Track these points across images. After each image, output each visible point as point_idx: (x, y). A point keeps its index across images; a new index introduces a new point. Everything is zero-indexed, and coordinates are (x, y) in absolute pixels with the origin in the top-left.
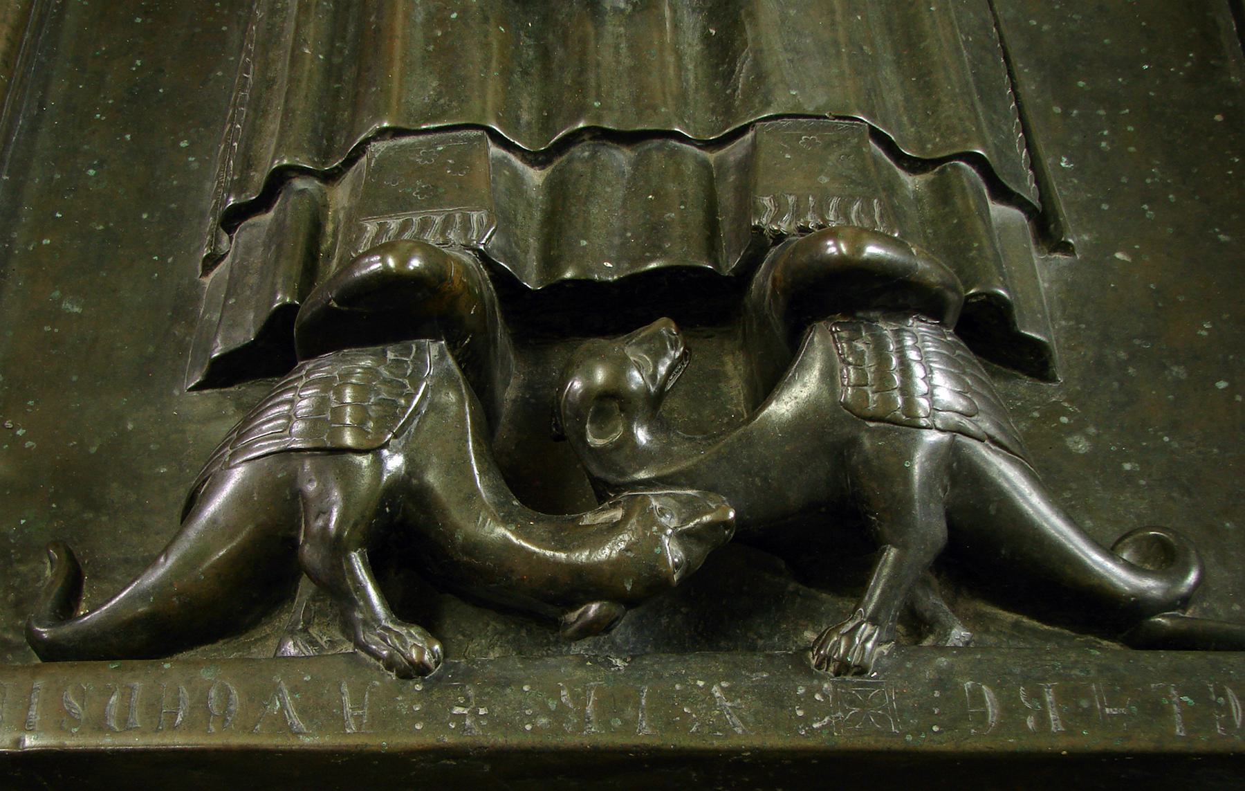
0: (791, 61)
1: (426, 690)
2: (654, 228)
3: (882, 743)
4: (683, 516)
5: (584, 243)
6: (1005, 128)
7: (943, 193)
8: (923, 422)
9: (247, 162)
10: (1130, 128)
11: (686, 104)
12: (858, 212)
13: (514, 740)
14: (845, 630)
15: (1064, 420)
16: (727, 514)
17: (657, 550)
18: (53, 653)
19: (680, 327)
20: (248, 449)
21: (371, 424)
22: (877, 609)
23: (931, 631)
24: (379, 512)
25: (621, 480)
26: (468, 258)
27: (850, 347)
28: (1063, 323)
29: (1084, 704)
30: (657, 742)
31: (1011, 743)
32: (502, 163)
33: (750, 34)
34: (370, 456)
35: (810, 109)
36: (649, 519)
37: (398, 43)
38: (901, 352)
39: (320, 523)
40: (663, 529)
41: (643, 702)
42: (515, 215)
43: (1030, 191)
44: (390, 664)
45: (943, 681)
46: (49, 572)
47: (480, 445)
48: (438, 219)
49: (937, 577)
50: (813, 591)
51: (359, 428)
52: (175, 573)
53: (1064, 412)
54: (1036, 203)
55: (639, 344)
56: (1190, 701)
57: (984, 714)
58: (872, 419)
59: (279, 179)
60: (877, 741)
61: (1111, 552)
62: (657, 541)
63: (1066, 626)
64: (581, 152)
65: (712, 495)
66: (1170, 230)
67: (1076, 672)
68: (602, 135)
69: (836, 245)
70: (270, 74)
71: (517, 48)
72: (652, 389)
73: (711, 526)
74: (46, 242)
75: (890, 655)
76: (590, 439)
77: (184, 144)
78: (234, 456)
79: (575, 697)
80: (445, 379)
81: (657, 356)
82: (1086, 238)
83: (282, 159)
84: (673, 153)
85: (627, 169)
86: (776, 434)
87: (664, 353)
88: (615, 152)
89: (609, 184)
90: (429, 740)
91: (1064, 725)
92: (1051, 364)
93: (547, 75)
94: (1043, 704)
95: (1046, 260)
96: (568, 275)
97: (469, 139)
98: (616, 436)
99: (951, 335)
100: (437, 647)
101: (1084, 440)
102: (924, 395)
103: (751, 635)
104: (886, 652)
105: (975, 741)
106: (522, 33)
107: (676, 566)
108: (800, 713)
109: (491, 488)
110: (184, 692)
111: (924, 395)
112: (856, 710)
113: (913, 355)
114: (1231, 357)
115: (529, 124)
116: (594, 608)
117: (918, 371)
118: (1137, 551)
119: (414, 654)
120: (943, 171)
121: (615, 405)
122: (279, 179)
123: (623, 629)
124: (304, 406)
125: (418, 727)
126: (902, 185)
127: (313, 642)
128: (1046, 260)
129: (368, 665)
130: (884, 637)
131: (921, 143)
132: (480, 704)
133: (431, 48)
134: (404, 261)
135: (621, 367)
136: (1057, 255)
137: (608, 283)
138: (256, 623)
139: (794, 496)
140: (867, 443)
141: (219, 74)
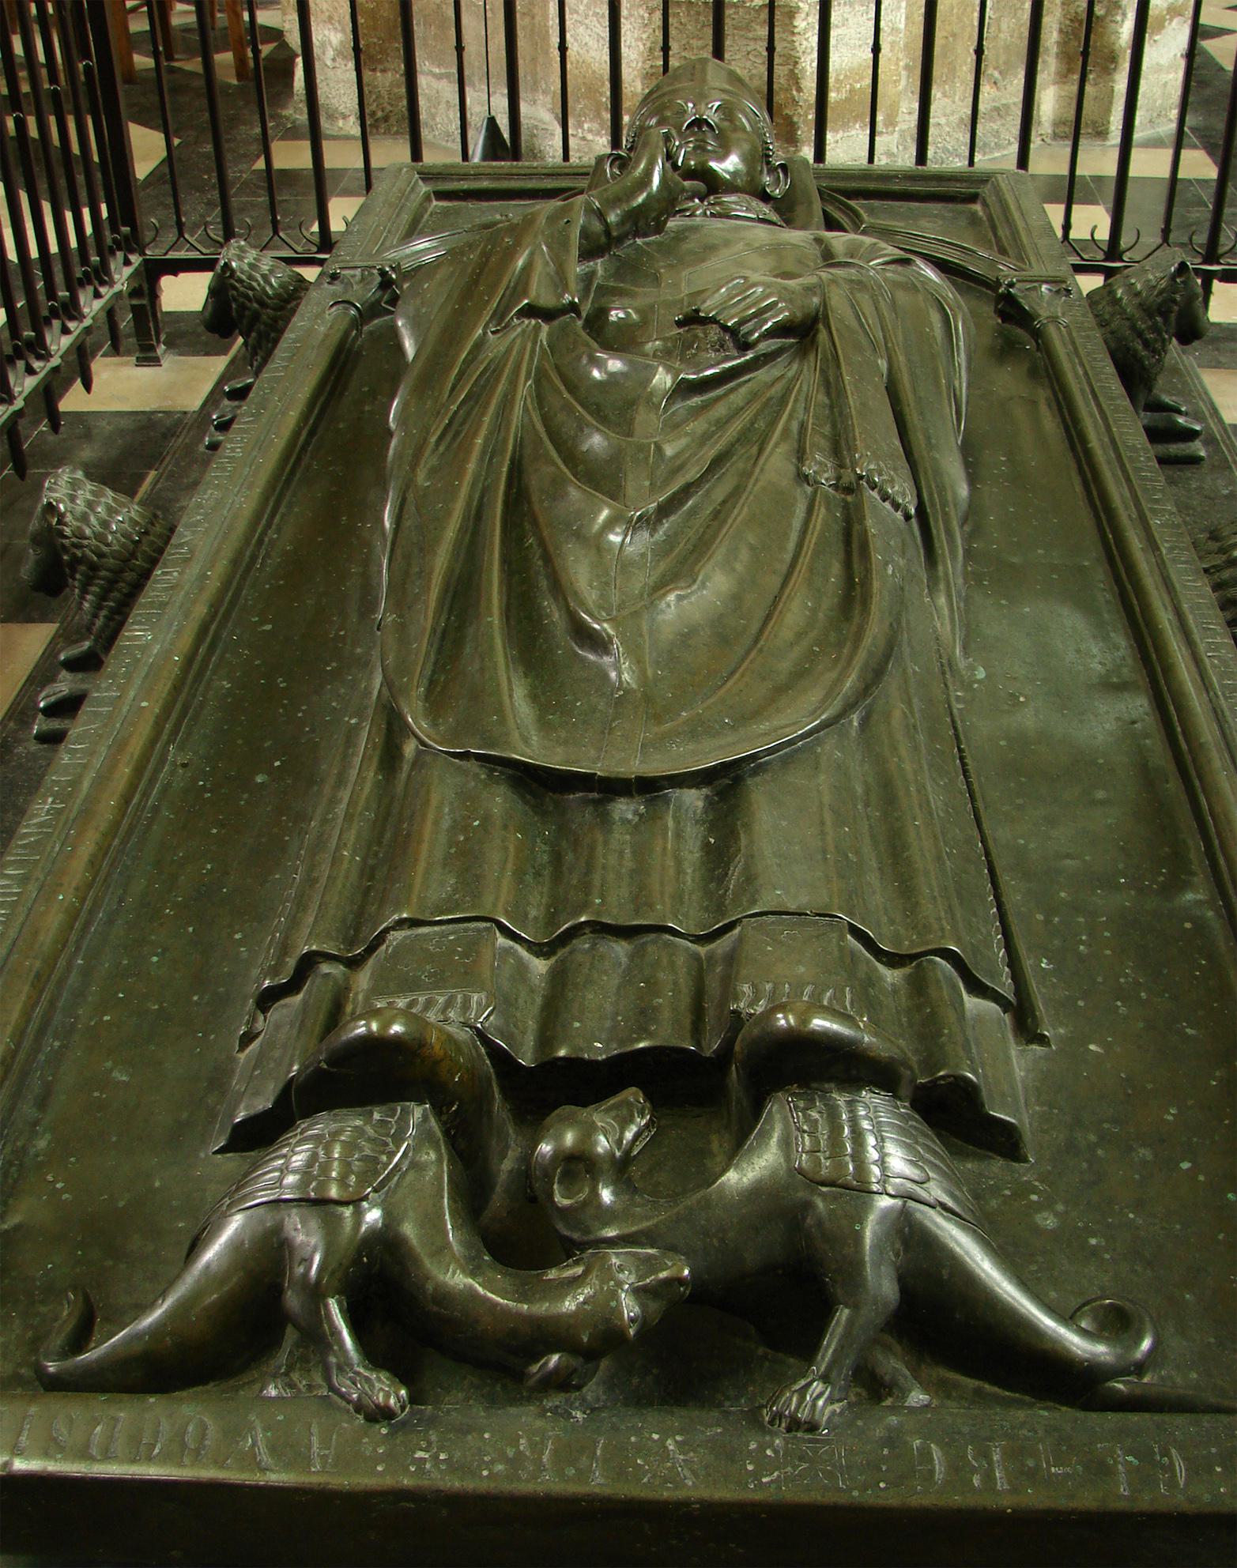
0: (779, 865)
1: (392, 1434)
2: (643, 1012)
3: (830, 1498)
4: (640, 1273)
5: (577, 1025)
6: (984, 930)
7: (918, 985)
8: (875, 1187)
9: (284, 949)
10: (1107, 934)
11: (682, 903)
12: (830, 997)
13: (470, 1485)
14: (797, 1387)
15: (1034, 1197)
16: (683, 1270)
17: (613, 1304)
18: (55, 1385)
19: (649, 1097)
20: (244, 1198)
21: (353, 1178)
22: (829, 1368)
23: (890, 1394)
24: (356, 1262)
25: (585, 1238)
26: (463, 1035)
27: (804, 1115)
28: (1037, 1108)
29: (1030, 1463)
30: (607, 1491)
31: (957, 1500)
32: (508, 951)
33: (743, 842)
34: (351, 1207)
35: (793, 907)
36: (607, 1273)
37: (425, 846)
38: (854, 1122)
39: (301, 1269)
40: (619, 1284)
41: (599, 1452)
42: (516, 999)
43: (1005, 985)
44: (359, 1407)
45: (893, 1440)
46: (67, 1314)
47: (455, 1202)
48: (441, 1000)
49: (900, 1342)
50: (780, 1355)
51: (342, 1181)
52: (171, 1315)
53: (1035, 1190)
54: (1011, 997)
55: (607, 1111)
56: (1136, 1462)
57: (932, 1472)
58: (823, 1184)
59: (308, 963)
60: (823, 1497)
61: (1068, 1318)
62: (614, 1295)
63: (1026, 1392)
64: (583, 944)
65: (671, 1254)
66: (1141, 1025)
67: (1025, 1432)
68: (602, 929)
69: (786, 1018)
70: (315, 874)
71: (532, 853)
72: (618, 1154)
73: (667, 1282)
74: (107, 1018)
75: (842, 1413)
76: (557, 1198)
77: (238, 936)
78: (230, 1206)
79: (532, 1445)
80: (425, 1137)
81: (625, 1123)
82: (1062, 1031)
83: (311, 946)
84: (668, 944)
85: (624, 960)
86: (733, 1197)
87: (631, 1121)
88: (614, 945)
89: (605, 972)
90: (389, 1482)
91: (1010, 1483)
92: (1022, 1145)
93: (557, 877)
94: (990, 1463)
95: (1024, 1051)
96: (562, 1053)
97: (478, 930)
98: (582, 1197)
99: (904, 1107)
100: (403, 1392)
101: (1052, 1217)
102: (875, 1163)
103: (719, 1396)
104: (838, 1411)
105: (919, 1497)
106: (538, 840)
107: (632, 1320)
108: (750, 1467)
109: (463, 1243)
110: (165, 1426)
111: (875, 1163)
112: (805, 1465)
113: (865, 1125)
114: (1195, 1140)
115: (536, 918)
116: (555, 1358)
117: (871, 1140)
118: (1095, 1319)
119: (381, 1398)
120: (919, 965)
121: (581, 1166)
122: (308, 963)
123: (594, 1387)
124: (298, 1160)
125: (380, 1468)
126: (881, 978)
127: (291, 1385)
128: (1024, 1051)
129: (339, 1408)
130: (837, 1396)
131: (897, 939)
132: (441, 1449)
133: (453, 851)
134: (387, 1025)
135: (588, 1132)
136: (1034, 1047)
137: (597, 1062)
138: (245, 1367)
139: (752, 1258)
140: (820, 1204)
141: (277, 876)
